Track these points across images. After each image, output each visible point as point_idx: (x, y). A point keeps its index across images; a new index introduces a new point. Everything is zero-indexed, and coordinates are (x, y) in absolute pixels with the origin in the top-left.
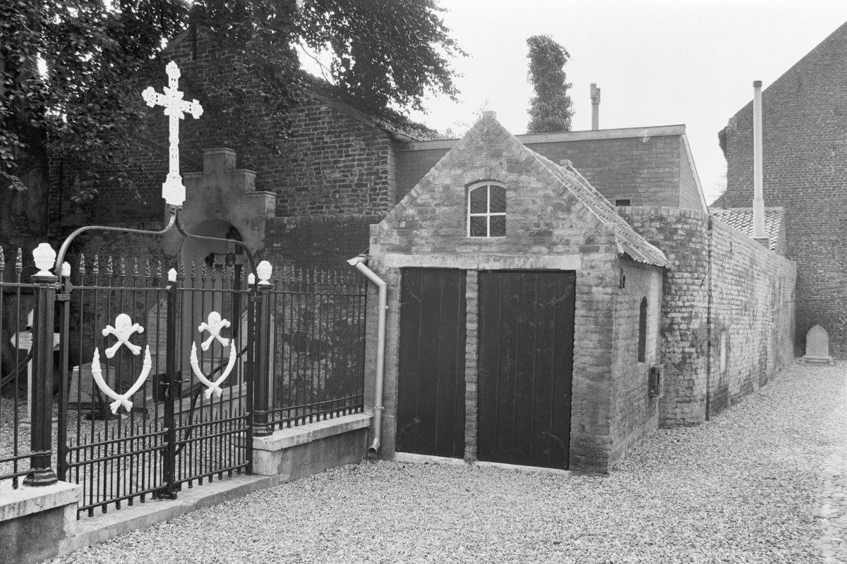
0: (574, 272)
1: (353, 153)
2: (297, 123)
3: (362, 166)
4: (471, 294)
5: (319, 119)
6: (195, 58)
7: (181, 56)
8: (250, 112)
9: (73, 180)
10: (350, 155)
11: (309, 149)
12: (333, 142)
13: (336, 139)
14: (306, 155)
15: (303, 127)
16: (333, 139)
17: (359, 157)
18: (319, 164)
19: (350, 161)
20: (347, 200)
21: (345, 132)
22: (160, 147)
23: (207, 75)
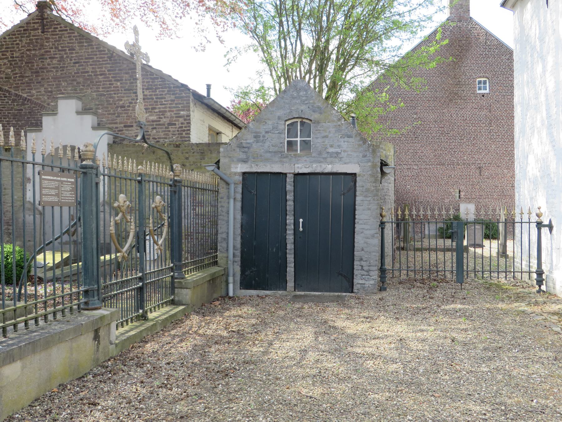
0: (355, 174)
1: (166, 103)
2: (124, 81)
3: (173, 111)
4: (289, 187)
6: (43, 32)
7: (31, 30)
8: (88, 72)
12: (150, 95)
13: (153, 93)
16: (151, 93)
17: (170, 106)
19: (164, 108)
20: (162, 134)
21: (159, 88)
22: (15, 94)
23: (53, 44)
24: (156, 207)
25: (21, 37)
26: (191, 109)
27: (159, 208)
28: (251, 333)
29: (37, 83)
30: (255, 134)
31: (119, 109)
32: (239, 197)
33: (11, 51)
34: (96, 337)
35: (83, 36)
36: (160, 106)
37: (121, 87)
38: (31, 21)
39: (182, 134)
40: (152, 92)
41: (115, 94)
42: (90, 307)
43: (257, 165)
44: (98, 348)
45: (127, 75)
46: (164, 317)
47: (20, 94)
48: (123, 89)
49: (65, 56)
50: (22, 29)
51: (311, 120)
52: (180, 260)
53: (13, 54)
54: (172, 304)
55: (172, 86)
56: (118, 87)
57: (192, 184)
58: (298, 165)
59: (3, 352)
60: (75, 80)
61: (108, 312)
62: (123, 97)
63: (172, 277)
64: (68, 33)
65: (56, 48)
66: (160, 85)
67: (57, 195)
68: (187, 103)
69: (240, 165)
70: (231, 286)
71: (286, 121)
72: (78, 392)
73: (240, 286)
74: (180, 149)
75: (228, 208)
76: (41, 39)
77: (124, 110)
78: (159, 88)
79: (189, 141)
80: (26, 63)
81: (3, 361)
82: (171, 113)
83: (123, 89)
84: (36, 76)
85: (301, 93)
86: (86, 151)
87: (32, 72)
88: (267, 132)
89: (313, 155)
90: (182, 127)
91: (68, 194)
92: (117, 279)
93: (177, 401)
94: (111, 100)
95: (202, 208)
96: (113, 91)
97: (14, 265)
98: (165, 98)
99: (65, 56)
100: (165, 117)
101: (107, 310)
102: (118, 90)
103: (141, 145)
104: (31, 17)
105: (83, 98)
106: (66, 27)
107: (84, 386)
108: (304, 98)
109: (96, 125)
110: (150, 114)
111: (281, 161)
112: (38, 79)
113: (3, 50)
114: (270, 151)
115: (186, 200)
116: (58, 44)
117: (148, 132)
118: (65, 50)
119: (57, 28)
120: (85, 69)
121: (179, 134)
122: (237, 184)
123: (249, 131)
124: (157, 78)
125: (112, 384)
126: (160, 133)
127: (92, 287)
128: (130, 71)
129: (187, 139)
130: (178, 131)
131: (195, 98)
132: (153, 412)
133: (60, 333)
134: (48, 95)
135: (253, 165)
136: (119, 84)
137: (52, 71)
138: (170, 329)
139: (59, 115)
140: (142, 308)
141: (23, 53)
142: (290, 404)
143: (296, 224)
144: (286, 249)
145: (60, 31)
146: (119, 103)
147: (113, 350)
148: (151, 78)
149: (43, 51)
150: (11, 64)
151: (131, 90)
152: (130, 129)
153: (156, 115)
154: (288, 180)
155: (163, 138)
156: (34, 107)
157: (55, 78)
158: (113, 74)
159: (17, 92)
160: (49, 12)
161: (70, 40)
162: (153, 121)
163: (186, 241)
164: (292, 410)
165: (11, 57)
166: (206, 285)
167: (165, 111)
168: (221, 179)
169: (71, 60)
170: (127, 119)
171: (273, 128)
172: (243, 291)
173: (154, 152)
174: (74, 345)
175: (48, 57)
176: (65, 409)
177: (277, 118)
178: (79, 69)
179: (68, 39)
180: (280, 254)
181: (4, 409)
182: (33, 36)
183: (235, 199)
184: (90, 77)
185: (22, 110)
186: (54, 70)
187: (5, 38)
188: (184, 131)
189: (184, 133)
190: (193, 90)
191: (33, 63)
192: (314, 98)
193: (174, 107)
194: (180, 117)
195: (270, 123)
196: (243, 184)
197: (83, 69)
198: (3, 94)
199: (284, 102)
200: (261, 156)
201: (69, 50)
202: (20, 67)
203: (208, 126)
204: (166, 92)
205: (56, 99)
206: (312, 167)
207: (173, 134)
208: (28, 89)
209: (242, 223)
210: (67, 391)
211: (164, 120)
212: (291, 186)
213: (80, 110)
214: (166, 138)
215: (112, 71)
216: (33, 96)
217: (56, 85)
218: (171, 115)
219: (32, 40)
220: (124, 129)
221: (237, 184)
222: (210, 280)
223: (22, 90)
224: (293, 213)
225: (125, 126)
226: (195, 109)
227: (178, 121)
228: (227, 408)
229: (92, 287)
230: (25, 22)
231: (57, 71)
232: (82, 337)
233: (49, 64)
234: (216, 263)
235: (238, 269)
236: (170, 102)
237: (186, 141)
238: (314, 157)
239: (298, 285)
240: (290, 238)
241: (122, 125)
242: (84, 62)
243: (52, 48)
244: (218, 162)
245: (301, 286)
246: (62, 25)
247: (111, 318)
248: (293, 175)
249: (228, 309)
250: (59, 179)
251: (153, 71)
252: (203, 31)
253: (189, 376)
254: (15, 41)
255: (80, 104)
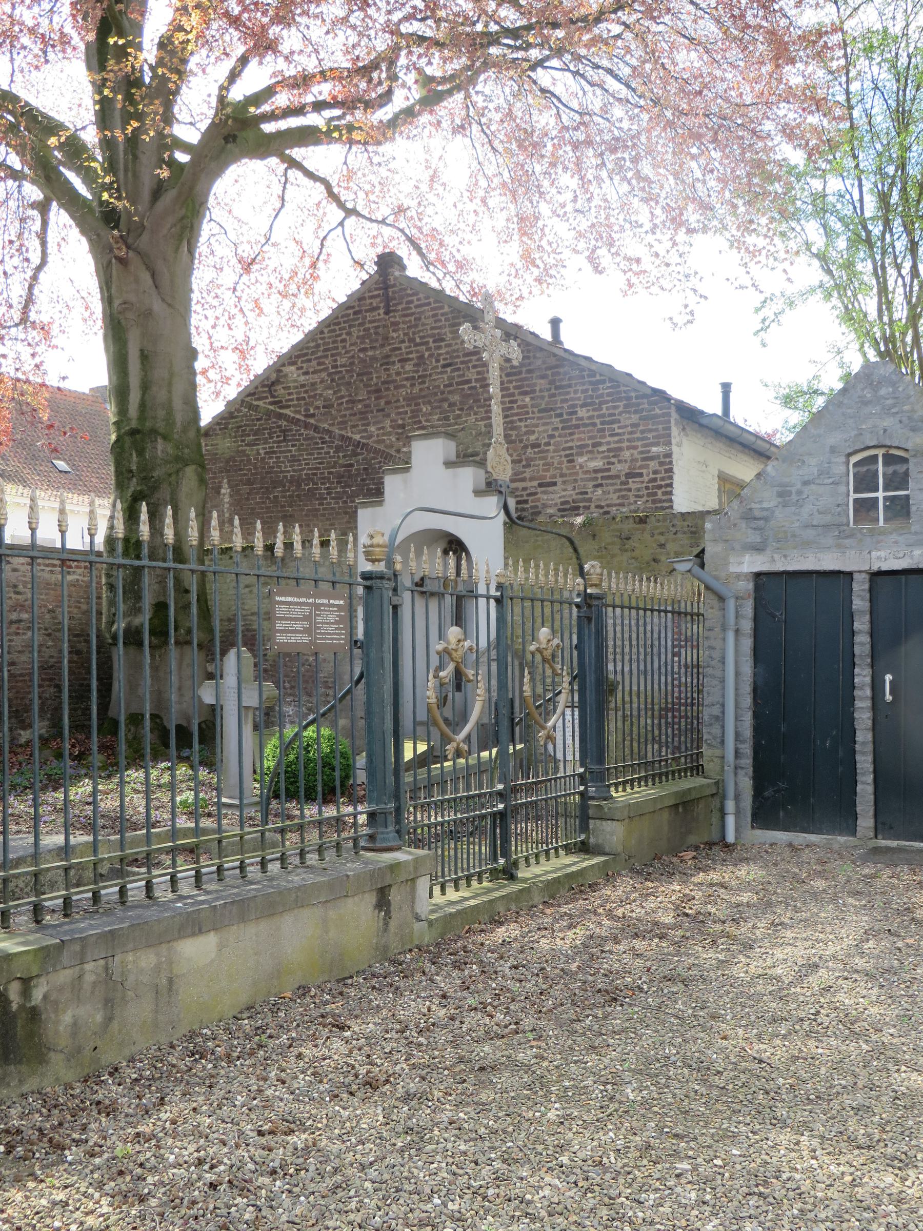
1: (620, 431)
3: (635, 448)
4: (860, 603)
5: (570, 386)
6: (386, 313)
7: (366, 311)
8: (468, 382)
9: (220, 487)
10: (617, 434)
11: (557, 429)
12: (590, 418)
13: (596, 413)
14: (551, 436)
15: (547, 399)
16: (591, 413)
18: (571, 448)
20: (615, 496)
21: (607, 402)
23: (405, 334)
24: (538, 650)
25: (350, 326)
26: (674, 441)
27: (548, 654)
28: (724, 922)
29: (378, 411)
30: (780, 489)
31: (529, 450)
32: (747, 626)
33: (332, 355)
34: (383, 902)
35: (459, 312)
36: (609, 439)
37: (532, 406)
38: (367, 295)
39: (655, 494)
40: (594, 410)
41: (520, 420)
42: (378, 845)
43: (785, 556)
44: (386, 924)
45: (542, 381)
46: (550, 877)
47: (349, 434)
48: (536, 410)
49: (427, 354)
50: (351, 311)
51: (907, 450)
52: (601, 761)
53: (336, 361)
54: (581, 851)
55: (633, 394)
56: (525, 406)
57: (626, 598)
58: (879, 553)
59: (180, 914)
60: (446, 400)
61: (410, 857)
62: (537, 426)
63: (582, 794)
64: (433, 309)
65: (410, 340)
66: (608, 395)
67: (308, 631)
68: (664, 429)
69: (747, 557)
70: (730, 821)
71: (850, 455)
72: (326, 1003)
73: (753, 822)
74: (648, 527)
75: (724, 650)
76: (385, 326)
77: (539, 452)
78: (607, 402)
79: (671, 507)
80: (358, 375)
81: (179, 930)
82: (632, 451)
83: (536, 410)
84: (377, 398)
85: (883, 392)
86: (372, 546)
87: (369, 392)
88: (806, 483)
89: (913, 529)
90: (655, 480)
91: (331, 629)
92: (444, 792)
93: (491, 1039)
94: (514, 433)
95: (695, 651)
96: (517, 414)
97: (320, 763)
98: (619, 422)
99: (427, 354)
100: (619, 461)
101: (410, 853)
102: (527, 413)
103: (567, 523)
104: (367, 286)
105: (459, 434)
106: (427, 298)
107: (341, 993)
108: (889, 402)
109: (483, 486)
110: (589, 456)
111: (839, 546)
112: (379, 405)
113: (320, 354)
114: (815, 523)
115: (663, 635)
116: (414, 333)
117: (586, 493)
118: (427, 343)
119: (411, 302)
120: (463, 375)
121: (649, 495)
122: (742, 598)
123: (766, 483)
124: (603, 382)
125: (390, 995)
126: (611, 496)
127: (383, 806)
128: (549, 372)
129: (667, 505)
130: (647, 488)
131: (682, 417)
132: (437, 1053)
133: (298, 889)
134: (397, 433)
135: (776, 556)
136: (527, 399)
137: (404, 386)
138: (561, 902)
139: (414, 471)
140: (506, 853)
141: (353, 357)
142: (708, 1069)
143: (876, 685)
144: (855, 742)
145: (416, 307)
146: (528, 440)
147: (422, 933)
148: (591, 383)
149: (388, 348)
150: (333, 380)
151: (551, 409)
152: (550, 489)
153: (602, 458)
154: (856, 587)
155: (616, 505)
156: (374, 458)
157: (410, 399)
158: (517, 381)
159: (343, 433)
160: (397, 273)
161: (436, 321)
162: (596, 471)
163: (663, 721)
164: (704, 1081)
165: (333, 367)
166: (666, 815)
167: (620, 449)
168: (707, 588)
169: (438, 361)
170: (544, 470)
171: (821, 473)
172: (758, 832)
173: (594, 536)
174: (332, 914)
175: (396, 359)
176: (289, 1031)
177: (828, 449)
178: (453, 378)
179: (431, 320)
180: (841, 754)
181: (182, 1016)
182: (370, 322)
183: (737, 631)
184: (473, 392)
185: (351, 465)
186: (408, 384)
187: (322, 332)
188: (660, 487)
189: (660, 492)
190: (676, 400)
191: (371, 373)
192: (912, 399)
193: (638, 439)
194: (651, 458)
195: (813, 461)
196: (755, 599)
197: (459, 376)
198: (321, 438)
199: (843, 414)
200: (794, 536)
201: (434, 342)
202: (349, 384)
203: (716, 473)
204: (621, 409)
205: (408, 440)
206: (912, 557)
207: (637, 496)
208: (363, 425)
209: (755, 683)
210: (308, 999)
211: (619, 467)
212: (863, 599)
213: (453, 457)
214: (622, 505)
215: (515, 374)
216: (371, 436)
217: (412, 411)
218: (632, 455)
219: (368, 329)
220: (539, 490)
221: (742, 598)
222: (676, 806)
223: (353, 426)
224: (869, 660)
225: (540, 485)
226: (685, 440)
227: (647, 466)
228: (576, 1062)
229: (383, 806)
230: (356, 296)
231: (413, 385)
232: (350, 901)
233: (398, 374)
234: (698, 770)
235: (746, 784)
236: (629, 429)
237: (663, 508)
238: (916, 533)
239: (884, 824)
240: (863, 717)
241: (535, 483)
242: (462, 363)
243: (403, 342)
244: (701, 555)
245: (891, 828)
246: (421, 296)
247: (416, 869)
248: (867, 577)
249: (705, 870)
250: (311, 600)
251: (594, 367)
252: (687, 276)
253: (541, 993)
254: (340, 335)
255: (452, 446)
